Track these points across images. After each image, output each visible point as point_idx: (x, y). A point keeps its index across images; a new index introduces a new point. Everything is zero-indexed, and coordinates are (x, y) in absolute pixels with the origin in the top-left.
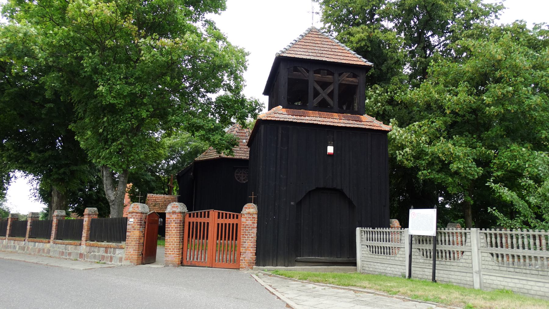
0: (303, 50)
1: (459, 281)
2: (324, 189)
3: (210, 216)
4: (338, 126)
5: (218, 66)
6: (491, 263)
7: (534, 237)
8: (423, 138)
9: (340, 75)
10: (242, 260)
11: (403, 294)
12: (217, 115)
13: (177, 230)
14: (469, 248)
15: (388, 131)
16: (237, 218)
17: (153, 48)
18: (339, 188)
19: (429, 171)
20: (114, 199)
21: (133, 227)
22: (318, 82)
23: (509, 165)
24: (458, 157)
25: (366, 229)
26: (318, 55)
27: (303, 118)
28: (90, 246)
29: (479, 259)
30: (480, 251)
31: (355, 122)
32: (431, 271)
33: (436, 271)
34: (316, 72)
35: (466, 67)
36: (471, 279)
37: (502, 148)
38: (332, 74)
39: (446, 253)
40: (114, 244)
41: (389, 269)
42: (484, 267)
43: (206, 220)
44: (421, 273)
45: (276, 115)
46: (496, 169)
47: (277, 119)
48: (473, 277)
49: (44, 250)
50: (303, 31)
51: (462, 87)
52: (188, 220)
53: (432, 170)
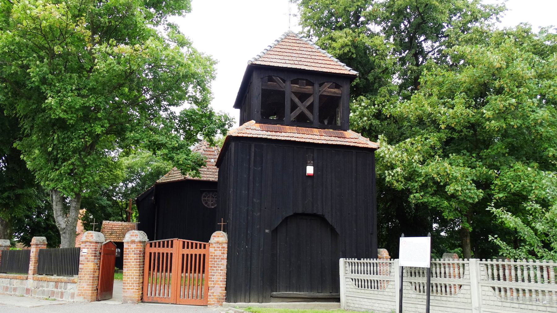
0: (279, 57)
3: (174, 246)
4: (318, 144)
6: (493, 298)
7: (541, 268)
8: (416, 156)
9: (321, 85)
12: (181, 131)
14: (467, 281)
15: (375, 149)
16: (205, 248)
18: (320, 213)
19: (422, 194)
21: (87, 258)
22: (295, 93)
23: (512, 186)
24: (456, 178)
25: (350, 260)
26: (296, 62)
27: (278, 134)
28: (38, 280)
30: (480, 284)
32: (425, 307)
34: (294, 82)
35: (464, 77)
38: (312, 84)
39: (441, 287)
41: (377, 305)
42: (484, 302)
45: (248, 131)
50: (279, 36)
52: (148, 250)
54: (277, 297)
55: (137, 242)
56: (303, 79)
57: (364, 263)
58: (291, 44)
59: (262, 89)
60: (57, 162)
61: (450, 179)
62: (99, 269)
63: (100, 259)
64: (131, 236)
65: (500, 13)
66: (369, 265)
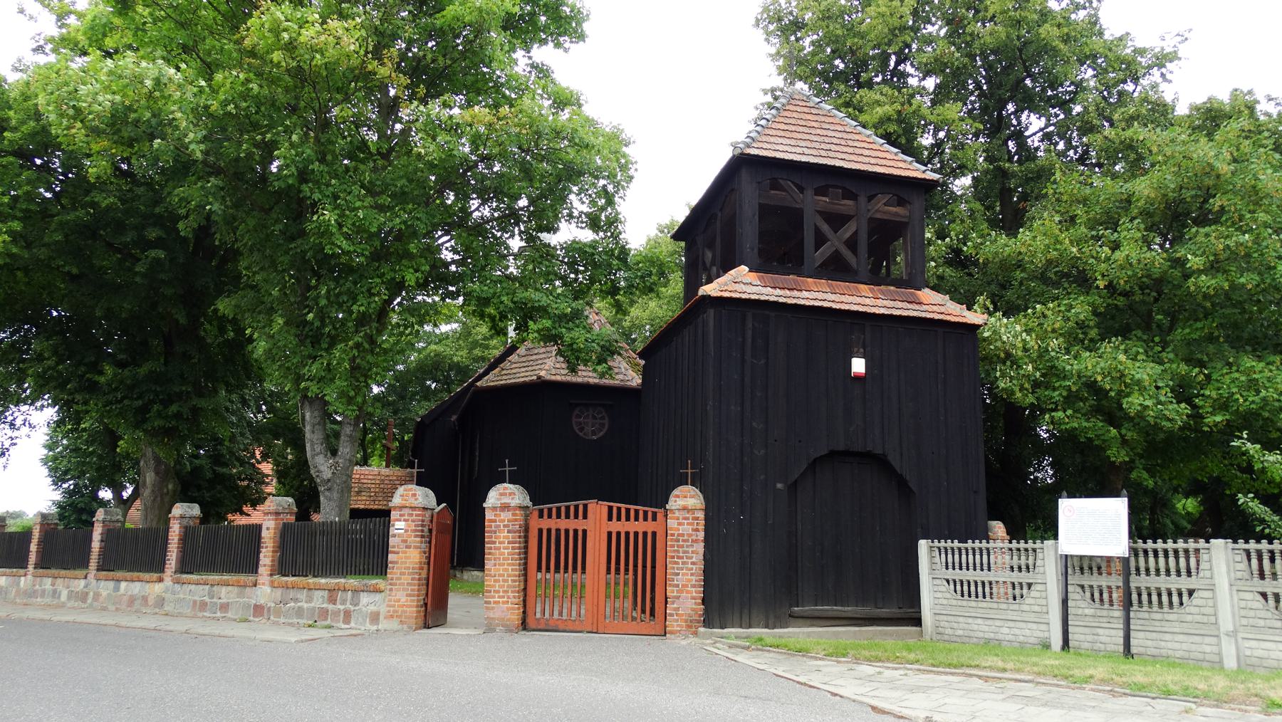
0: (788, 142)
1: (1187, 655)
2: (846, 454)
3: (590, 514)
4: (874, 314)
5: (560, 165)
6: (1263, 614)
7: (1156, 552)
9: (870, 198)
10: (672, 615)
11: (1103, 681)
13: (513, 548)
14: (1207, 581)
15: (978, 326)
16: (654, 519)
17: (444, 124)
18: (878, 451)
19: (1069, 412)
20: (330, 476)
21: (405, 541)
24: (1139, 382)
25: (943, 544)
27: (795, 293)
29: (1233, 606)
30: (1235, 588)
31: (909, 306)
32: (1121, 633)
33: (1132, 634)
34: (820, 191)
35: (1143, 187)
36: (1215, 649)
37: (1219, 365)
38: (853, 197)
40: (352, 582)
41: (1005, 630)
42: (1244, 622)
43: (580, 524)
44: (1090, 638)
45: (737, 287)
46: (1210, 410)
47: (744, 296)
48: (1219, 644)
49: (145, 599)
51: (1130, 231)
52: (536, 524)
53: (1075, 411)
54: (802, 617)
55: (516, 508)
56: (837, 187)
57: (974, 549)
58: (802, 116)
59: (761, 206)
60: (319, 342)
61: (1128, 386)
62: (429, 564)
63: (430, 542)
64: (501, 494)
65: (1168, 64)
66: (950, 552)
